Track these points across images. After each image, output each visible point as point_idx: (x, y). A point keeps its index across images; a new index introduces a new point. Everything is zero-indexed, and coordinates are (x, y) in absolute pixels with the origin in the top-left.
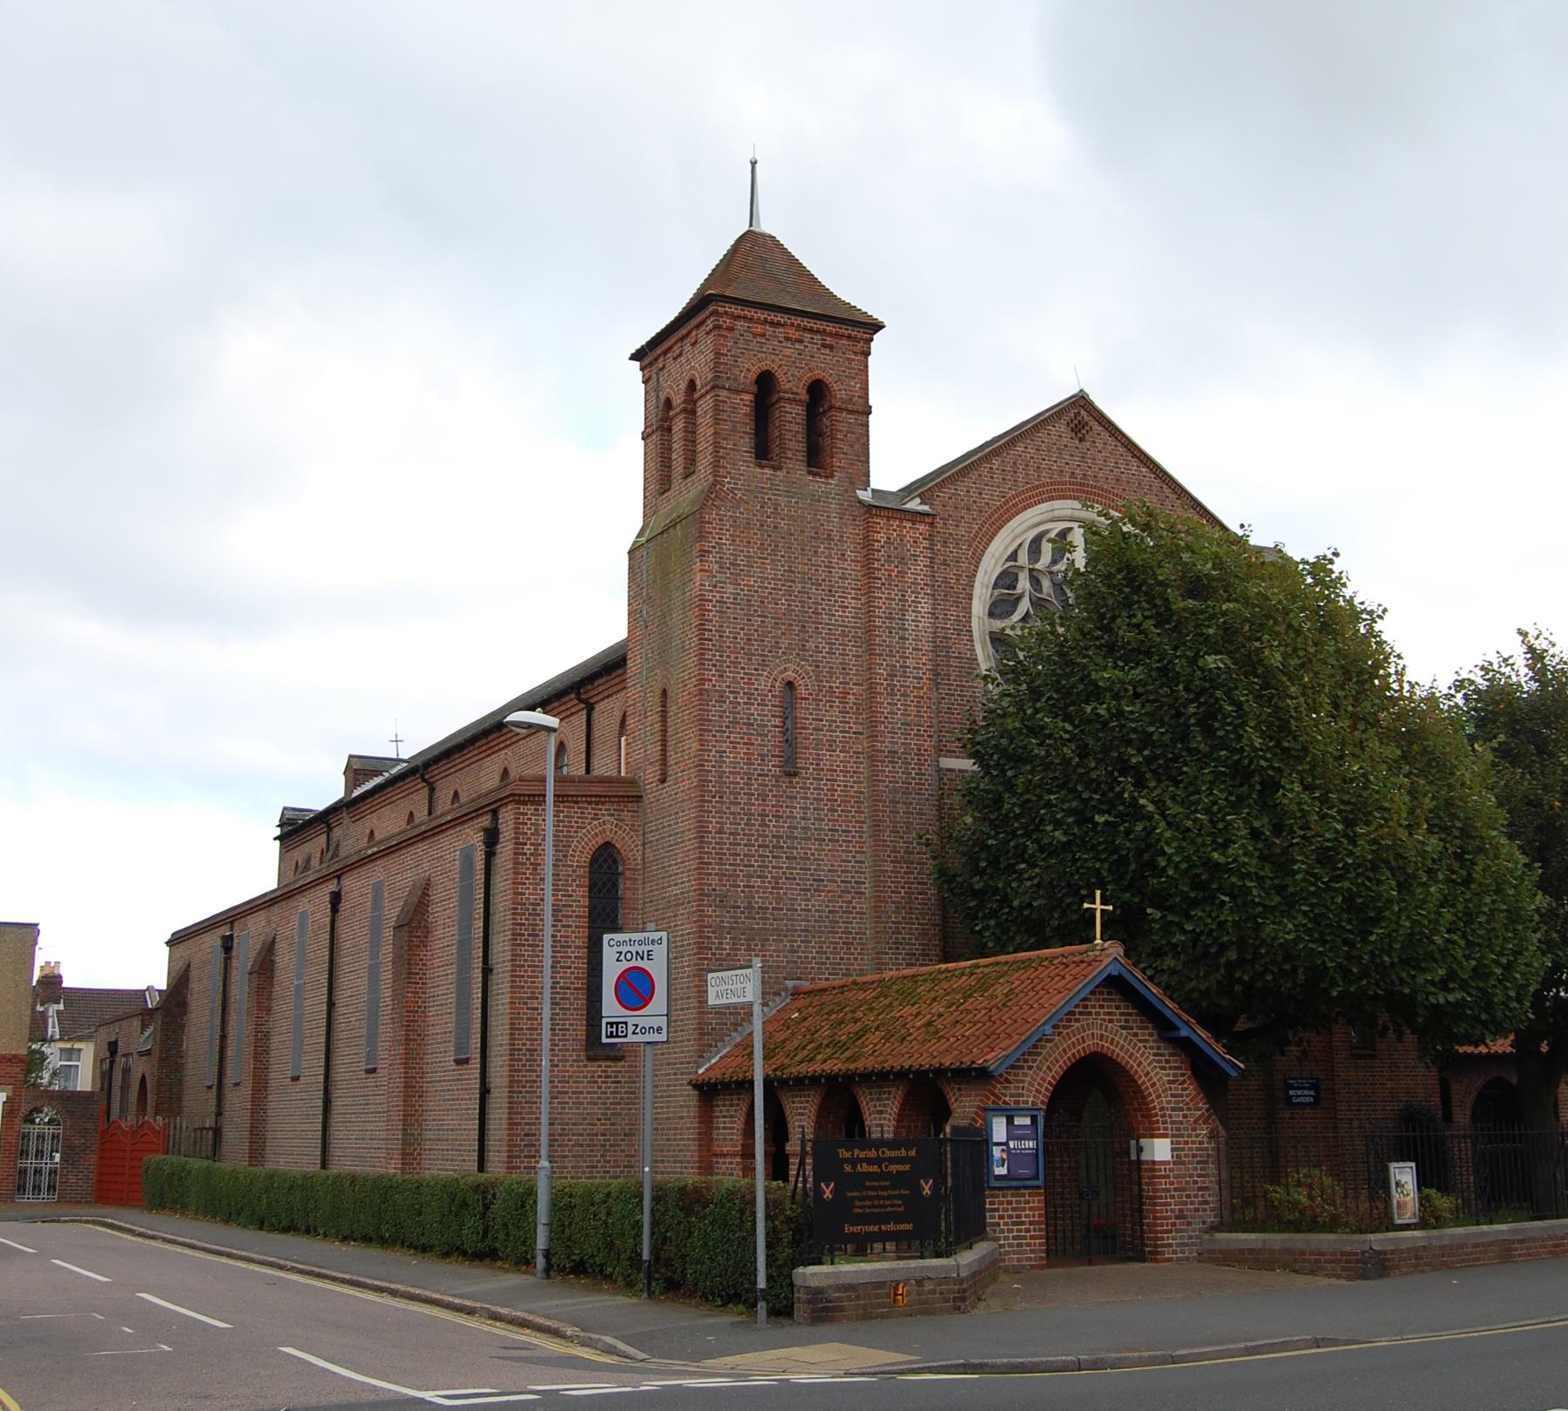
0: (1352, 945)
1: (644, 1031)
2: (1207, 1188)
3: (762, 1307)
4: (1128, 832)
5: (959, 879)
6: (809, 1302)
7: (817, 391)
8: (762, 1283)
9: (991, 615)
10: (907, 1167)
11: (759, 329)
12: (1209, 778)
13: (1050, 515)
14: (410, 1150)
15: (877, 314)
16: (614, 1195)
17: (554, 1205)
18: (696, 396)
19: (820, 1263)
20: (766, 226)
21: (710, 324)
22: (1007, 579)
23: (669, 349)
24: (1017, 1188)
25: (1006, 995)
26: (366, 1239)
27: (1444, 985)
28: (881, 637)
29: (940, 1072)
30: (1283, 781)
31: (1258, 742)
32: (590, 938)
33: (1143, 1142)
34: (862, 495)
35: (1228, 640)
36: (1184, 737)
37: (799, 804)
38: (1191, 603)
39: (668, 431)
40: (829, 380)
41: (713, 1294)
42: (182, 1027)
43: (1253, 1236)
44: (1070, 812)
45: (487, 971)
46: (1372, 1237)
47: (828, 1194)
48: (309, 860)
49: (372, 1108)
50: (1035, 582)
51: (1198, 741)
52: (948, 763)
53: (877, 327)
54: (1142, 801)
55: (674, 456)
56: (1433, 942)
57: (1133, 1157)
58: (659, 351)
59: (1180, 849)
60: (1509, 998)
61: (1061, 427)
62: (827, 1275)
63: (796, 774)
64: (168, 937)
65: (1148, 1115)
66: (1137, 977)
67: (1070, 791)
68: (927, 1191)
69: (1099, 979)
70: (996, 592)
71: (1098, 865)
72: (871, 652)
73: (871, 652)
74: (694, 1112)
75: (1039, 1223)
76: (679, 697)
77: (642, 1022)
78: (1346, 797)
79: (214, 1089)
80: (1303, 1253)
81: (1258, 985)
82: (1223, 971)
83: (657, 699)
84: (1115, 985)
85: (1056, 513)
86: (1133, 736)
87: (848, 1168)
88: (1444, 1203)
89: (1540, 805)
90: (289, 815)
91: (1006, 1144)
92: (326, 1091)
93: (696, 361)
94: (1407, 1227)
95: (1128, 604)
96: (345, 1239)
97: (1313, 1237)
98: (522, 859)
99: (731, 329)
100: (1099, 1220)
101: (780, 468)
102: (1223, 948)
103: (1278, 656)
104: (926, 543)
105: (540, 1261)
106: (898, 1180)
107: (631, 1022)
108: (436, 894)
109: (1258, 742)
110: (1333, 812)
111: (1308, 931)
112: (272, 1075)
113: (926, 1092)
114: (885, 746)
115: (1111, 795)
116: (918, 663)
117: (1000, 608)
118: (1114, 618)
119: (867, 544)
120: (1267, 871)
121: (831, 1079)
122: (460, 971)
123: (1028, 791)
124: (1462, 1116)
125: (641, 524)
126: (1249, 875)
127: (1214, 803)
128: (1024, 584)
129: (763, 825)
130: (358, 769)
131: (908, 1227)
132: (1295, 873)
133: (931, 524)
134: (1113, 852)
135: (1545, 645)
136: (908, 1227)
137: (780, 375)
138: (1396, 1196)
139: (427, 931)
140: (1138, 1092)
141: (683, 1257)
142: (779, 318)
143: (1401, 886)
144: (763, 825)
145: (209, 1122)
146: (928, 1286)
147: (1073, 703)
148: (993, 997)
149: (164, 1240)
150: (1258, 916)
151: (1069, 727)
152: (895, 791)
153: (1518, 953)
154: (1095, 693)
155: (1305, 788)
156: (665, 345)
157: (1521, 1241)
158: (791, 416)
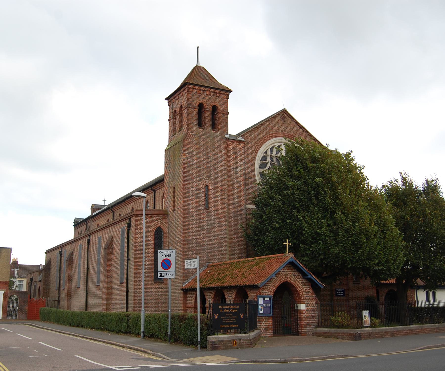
3: (199, 346)
4: (295, 225)
6: (211, 345)
7: (215, 108)
8: (199, 340)
9: (260, 168)
10: (237, 311)
11: (199, 92)
12: (317, 210)
13: (276, 141)
14: (108, 306)
17: (146, 320)
18: (183, 109)
19: (214, 335)
20: (201, 64)
22: (264, 158)
23: (184, 90)
24: (266, 316)
26: (97, 329)
28: (231, 173)
29: (246, 286)
30: (336, 211)
31: (330, 201)
32: (155, 251)
33: (298, 305)
35: (322, 174)
36: (311, 200)
38: (313, 164)
39: (175, 118)
40: (218, 105)
42: (49, 274)
43: (327, 329)
44: (280, 219)
45: (128, 260)
46: (358, 330)
47: (216, 317)
48: (82, 231)
50: (272, 160)
51: (314, 201)
52: (248, 206)
53: (231, 91)
54: (299, 216)
56: (375, 254)
57: (296, 309)
58: (173, 97)
59: (309, 229)
63: (208, 209)
66: (297, 262)
68: (242, 317)
69: (287, 263)
70: (261, 162)
72: (228, 177)
73: (228, 177)
76: (178, 189)
78: (353, 216)
80: (339, 334)
82: (320, 261)
83: (172, 189)
84: (292, 264)
85: (278, 141)
86: (297, 199)
87: (221, 311)
88: (377, 321)
89: (404, 218)
90: (77, 220)
91: (263, 305)
92: (87, 291)
93: (183, 100)
95: (296, 165)
97: (342, 329)
98: (137, 231)
99: (192, 92)
100: (286, 324)
101: (205, 129)
102: (320, 255)
103: (336, 178)
106: (234, 314)
107: (165, 273)
108: (115, 240)
109: (330, 201)
110: (349, 220)
111: (342, 251)
113: (242, 291)
114: (232, 201)
116: (241, 181)
117: (262, 166)
118: (292, 168)
119: (227, 149)
120: (332, 235)
123: (269, 214)
124: (382, 299)
128: (269, 160)
129: (200, 222)
130: (78, 223)
131: (237, 326)
132: (339, 235)
133: (244, 144)
136: (237, 326)
137: (205, 104)
139: (113, 250)
140: (297, 291)
141: (179, 333)
142: (204, 89)
143: (367, 239)
144: (200, 222)
145: (57, 299)
146: (242, 341)
147: (281, 191)
149: (45, 329)
150: (329, 246)
151: (280, 197)
152: (234, 213)
153: (397, 257)
154: (287, 188)
155: (342, 213)
157: (396, 331)
158: (208, 115)
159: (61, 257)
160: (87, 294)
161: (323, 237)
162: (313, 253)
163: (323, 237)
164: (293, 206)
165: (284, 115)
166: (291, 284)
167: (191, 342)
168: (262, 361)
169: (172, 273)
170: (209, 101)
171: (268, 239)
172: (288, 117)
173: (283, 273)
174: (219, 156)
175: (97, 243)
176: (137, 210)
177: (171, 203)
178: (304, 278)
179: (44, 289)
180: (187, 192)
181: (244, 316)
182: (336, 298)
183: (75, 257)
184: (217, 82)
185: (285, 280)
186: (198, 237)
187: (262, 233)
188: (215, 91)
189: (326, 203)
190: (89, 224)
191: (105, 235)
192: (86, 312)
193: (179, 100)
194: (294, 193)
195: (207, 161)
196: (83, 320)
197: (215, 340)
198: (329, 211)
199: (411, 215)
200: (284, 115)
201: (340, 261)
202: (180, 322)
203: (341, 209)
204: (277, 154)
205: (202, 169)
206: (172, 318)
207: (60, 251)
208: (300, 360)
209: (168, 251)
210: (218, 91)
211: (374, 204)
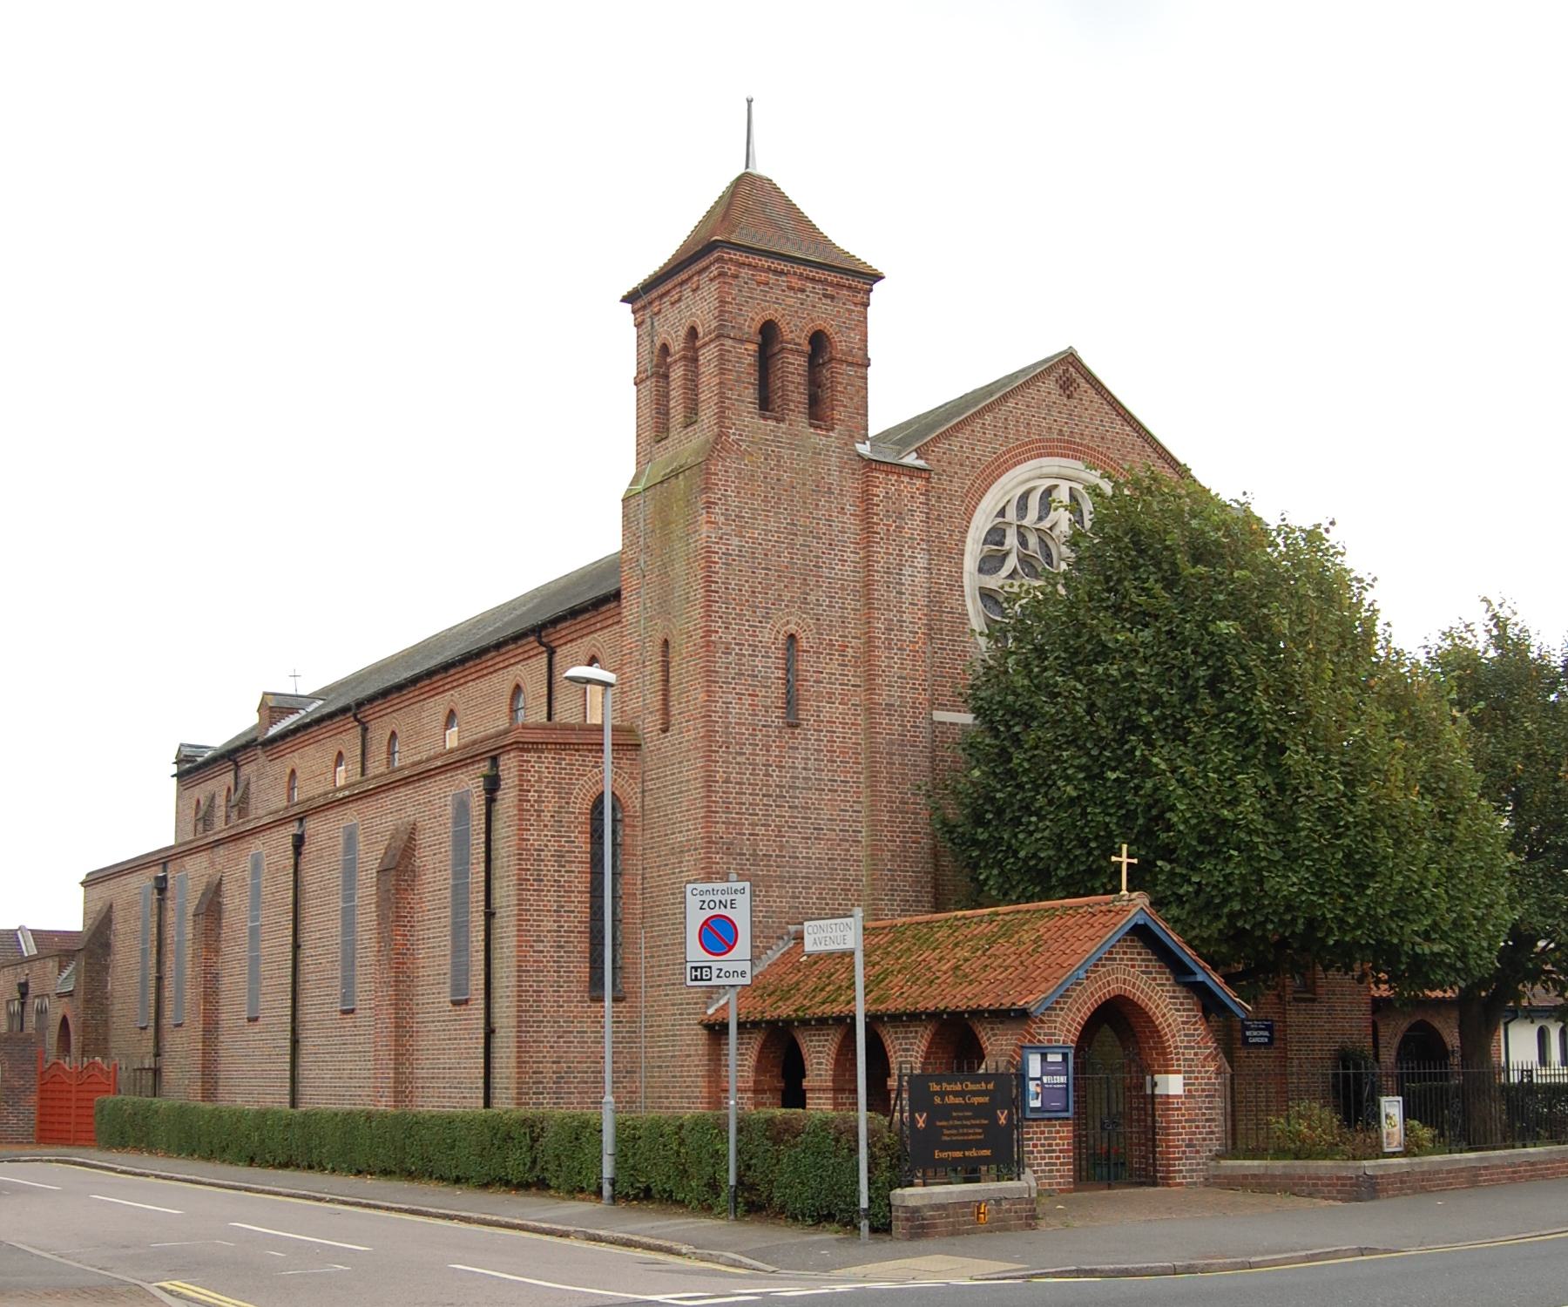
0: (1349, 898)
1: (728, 975)
2: (1213, 1120)
3: (864, 1224)
4: (1137, 788)
5: (960, 830)
6: (907, 1219)
7: (818, 340)
8: (864, 1203)
9: (980, 570)
10: (987, 1099)
11: (763, 276)
12: (1218, 739)
13: (1038, 472)
14: (402, 1089)
15: (875, 262)
16: (688, 1126)
17: (619, 1140)
18: (698, 344)
19: (911, 1185)
20: (761, 168)
21: (714, 271)
22: (996, 535)
24: (1049, 1119)
25: (1035, 942)
26: (386, 1173)
27: (1427, 937)
28: (880, 592)
29: (977, 1013)
30: (1288, 743)
31: (1266, 706)
32: (592, 883)
33: (1157, 1077)
34: (864, 449)
35: (1236, 607)
36: (1191, 698)
37: (801, 754)
38: (1201, 569)
39: (665, 378)
40: (830, 331)
41: (804, 1215)
42: (106, 968)
43: (1256, 1163)
44: (1080, 768)
45: (489, 915)
46: (1365, 1163)
47: (921, 1124)
48: (213, 797)
49: (351, 1048)
50: (1023, 542)
51: (1207, 704)
52: (939, 716)
53: (878, 277)
54: (1155, 760)
55: (672, 404)
56: (1421, 896)
57: (1149, 1092)
58: (654, 294)
59: (1191, 806)
60: (1483, 948)
61: (1050, 384)
62: (922, 1196)
63: (797, 726)
64: (83, 877)
65: (1164, 1053)
66: (1162, 928)
67: (1080, 748)
68: (1003, 1121)
69: (1127, 928)
70: (987, 547)
71: (1107, 819)
72: (869, 604)
73: (869, 604)
74: (702, 1050)
75: (1067, 1151)
76: (683, 649)
77: (726, 967)
78: (1345, 760)
79: (151, 1031)
80: (1302, 1178)
81: (1258, 933)
82: (1225, 920)
83: (658, 649)
84: (1140, 933)
85: (1045, 471)
86: (1144, 697)
87: (938, 1100)
89: (1503, 767)
90: (187, 751)
92: (294, 1031)
93: (698, 306)
94: (1393, 1155)
95: (1135, 568)
96: (359, 1172)
97: (1310, 1163)
98: (526, 806)
99: (736, 277)
100: (1119, 1149)
101: (783, 420)
102: (1227, 899)
103: (1286, 623)
104: (922, 499)
105: (607, 1189)
106: (979, 1111)
107: (715, 966)
108: (423, 839)
109: (1266, 706)
110: (1333, 773)
111: (1310, 884)
112: (223, 1016)
113: (958, 1036)
114: (882, 698)
115: (1120, 752)
116: (914, 619)
117: (990, 564)
118: (1120, 581)
119: (866, 499)
120: (1270, 828)
121: (772, 1024)
122: (455, 914)
123: (1036, 748)
124: (1388, 1057)
125: (633, 471)
126: (1256, 831)
127: (1222, 762)
128: (1011, 540)
130: (193, 768)
131: (987, 1153)
132: (1297, 831)
133: (928, 480)
134: (1120, 807)
135: (1508, 613)
136: (987, 1153)
137: (782, 325)
138: (1385, 1126)
139: (415, 875)
140: (1156, 1032)
141: (771, 1182)
142: (782, 266)
143: (1397, 843)
145: (148, 1062)
146: (1005, 1206)
147: (1080, 663)
148: (1020, 942)
149: (157, 1176)
150: (1262, 869)
151: (1080, 687)
152: (891, 743)
153: (1490, 906)
154: (1103, 653)
155: (1309, 750)
156: (662, 290)
157: (1486, 1168)
158: (794, 366)
159: (161, 902)
160: (295, 1043)
161: (1242, 835)
162: (1197, 893)
163: (1242, 835)
164: (1128, 720)
165: (1067, 372)
166: (1135, 1004)
167: (830, 1212)
168: (1112, 1271)
169: (740, 967)
170: (798, 314)
171: (1035, 840)
172: (1081, 381)
173: (1111, 965)
174: (836, 526)
175: (340, 848)
176: (525, 727)
177: (655, 701)
178: (1178, 983)
179: (85, 1025)
180: (721, 660)
181: (1009, 1118)
182: (1243, 1053)
183: (234, 901)
184: (826, 243)
185: (1115, 988)
186: (761, 830)
187: (1008, 816)
188: (820, 274)
189: (1251, 712)
190: (246, 770)
191: (377, 824)
192: (209, 1106)
193: (682, 304)
194: (1131, 674)
195: (792, 545)
196: (313, 1144)
197: (919, 1203)
198: (1263, 740)
199: (1528, 757)
200: (1067, 372)
201: (1301, 921)
202: (777, 1140)
203: (1303, 735)
204: (1040, 519)
205: (773, 574)
206: (739, 1131)
207: (157, 878)
208: (1235, 1266)
209: (724, 886)
210: (832, 277)
211: (1411, 715)
